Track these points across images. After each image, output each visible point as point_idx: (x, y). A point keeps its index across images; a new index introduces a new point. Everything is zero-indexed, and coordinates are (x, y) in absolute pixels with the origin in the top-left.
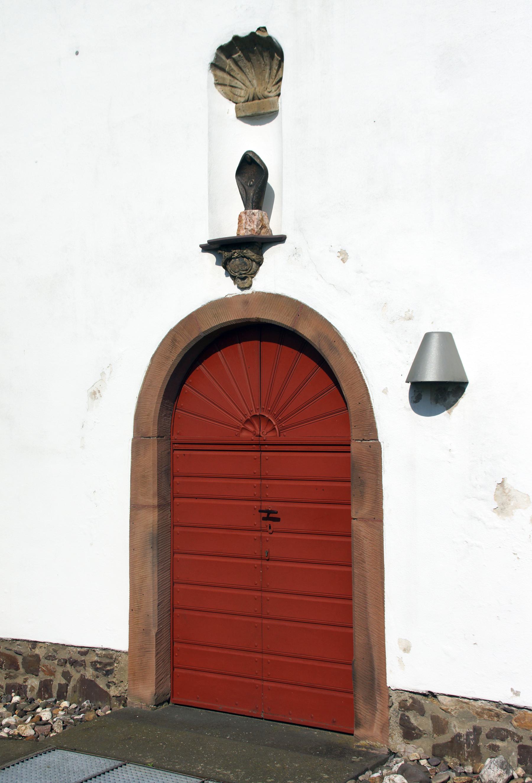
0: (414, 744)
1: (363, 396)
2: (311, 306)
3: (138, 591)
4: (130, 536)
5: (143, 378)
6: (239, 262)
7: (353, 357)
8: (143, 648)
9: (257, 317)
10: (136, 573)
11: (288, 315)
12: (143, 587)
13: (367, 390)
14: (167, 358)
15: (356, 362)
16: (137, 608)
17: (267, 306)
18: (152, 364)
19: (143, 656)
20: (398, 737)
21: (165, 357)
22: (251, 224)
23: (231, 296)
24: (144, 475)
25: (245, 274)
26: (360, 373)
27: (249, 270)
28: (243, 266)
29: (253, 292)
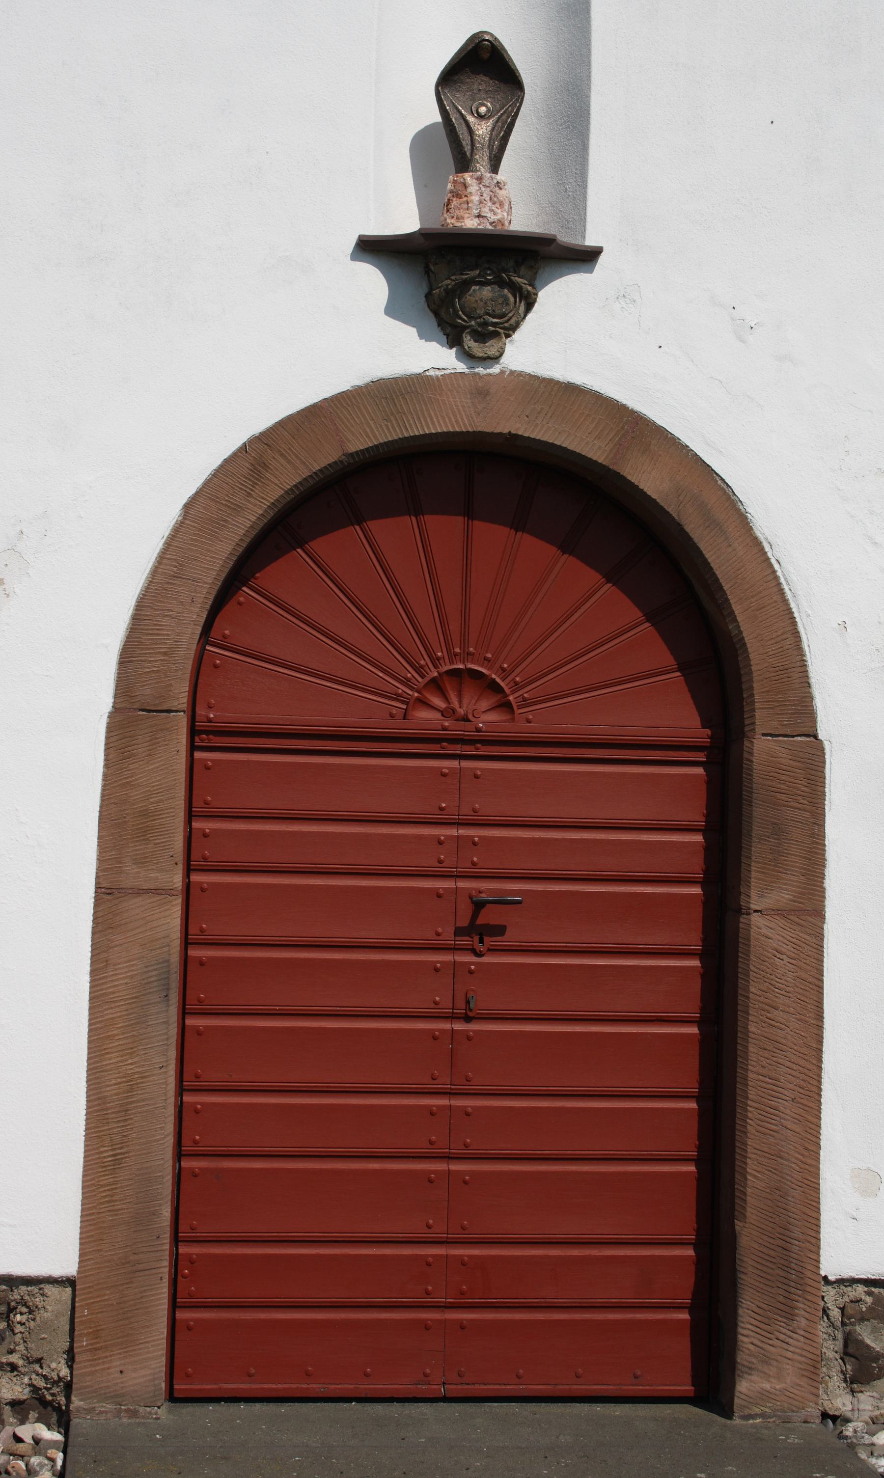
0: (873, 1392)
1: (784, 637)
2: (659, 422)
3: (113, 1116)
4: (93, 973)
5: (155, 555)
6: (490, 295)
7: (763, 549)
8: (128, 1263)
9: (513, 432)
10: (108, 1067)
11: (598, 437)
12: (131, 1103)
13: (794, 623)
14: (237, 509)
15: (768, 559)
16: (110, 1159)
17: (542, 409)
18: (187, 522)
19: (127, 1283)
20: (837, 1382)
21: (229, 507)
22: (494, 208)
23: (439, 373)
24: (147, 810)
25: (495, 325)
26: (779, 584)
27: (507, 318)
28: (500, 306)
29: (502, 372)
